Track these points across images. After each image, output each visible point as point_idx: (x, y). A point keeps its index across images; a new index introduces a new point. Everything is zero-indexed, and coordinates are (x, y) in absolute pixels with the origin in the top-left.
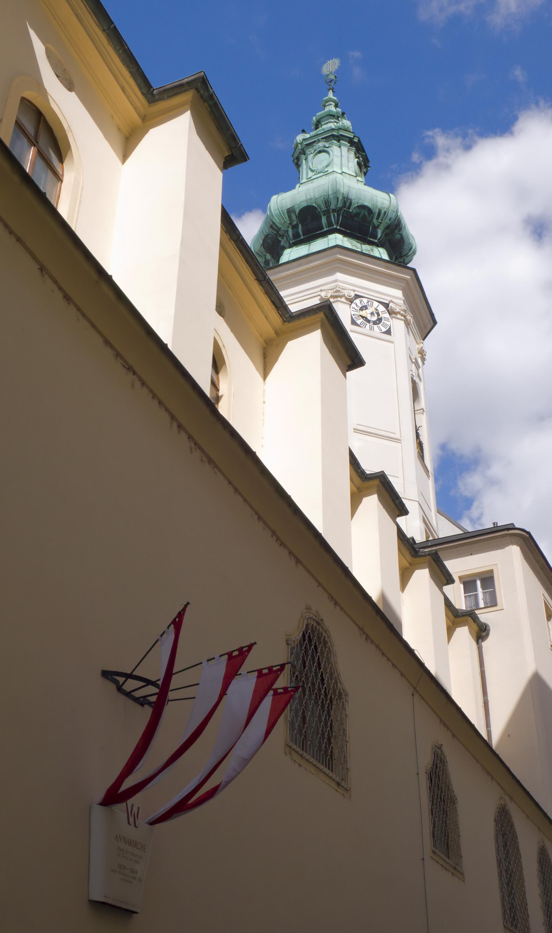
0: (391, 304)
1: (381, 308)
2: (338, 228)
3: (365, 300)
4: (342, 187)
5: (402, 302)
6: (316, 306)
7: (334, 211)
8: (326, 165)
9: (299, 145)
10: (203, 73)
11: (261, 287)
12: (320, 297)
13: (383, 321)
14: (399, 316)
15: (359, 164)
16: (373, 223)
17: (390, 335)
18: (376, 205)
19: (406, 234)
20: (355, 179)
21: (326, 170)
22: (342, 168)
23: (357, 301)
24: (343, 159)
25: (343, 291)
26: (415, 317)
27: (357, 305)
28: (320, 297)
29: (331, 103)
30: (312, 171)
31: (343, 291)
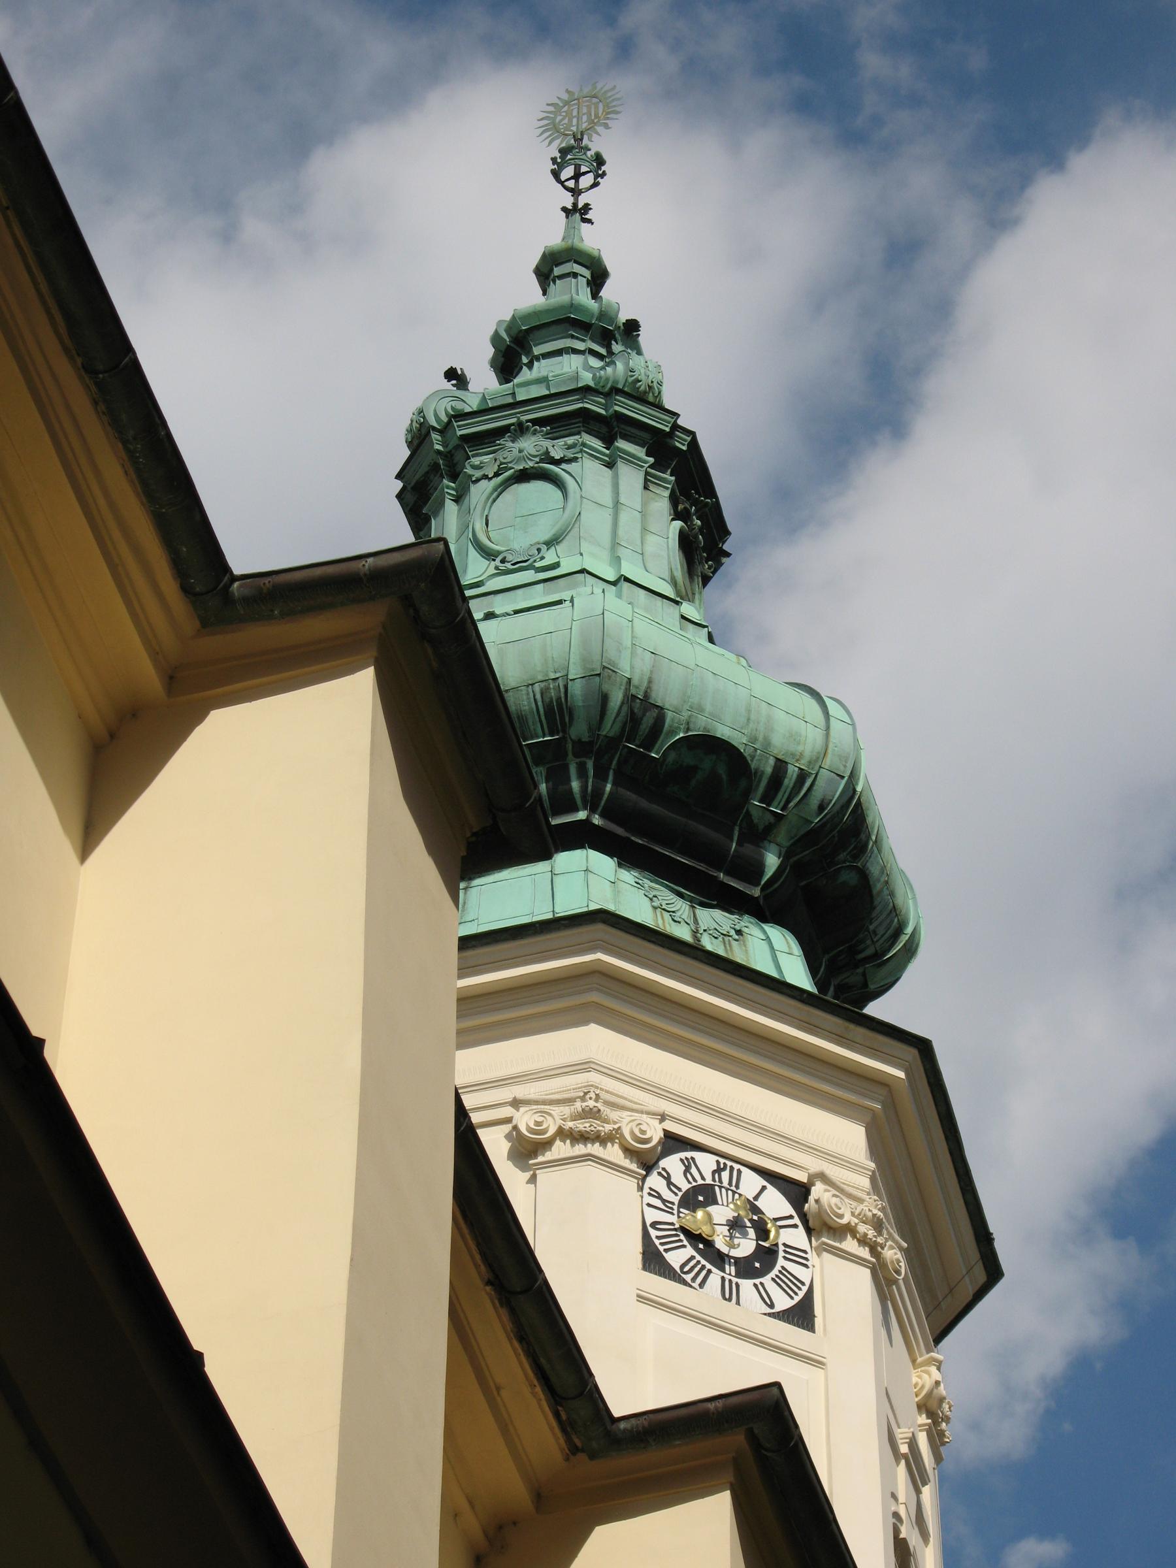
0: (818, 1191)
1: (775, 1204)
2: (597, 820)
3: (706, 1163)
4: (626, 654)
5: (865, 1183)
6: (719, 1404)
7: (583, 749)
8: (547, 536)
9: (435, 436)
10: (441, 546)
11: (504, 1312)
12: (507, 1128)
13: (781, 1262)
14: (850, 1245)
15: (686, 542)
16: (748, 814)
17: (814, 1332)
18: (767, 743)
19: (883, 868)
20: (671, 614)
21: (550, 558)
22: (616, 561)
23: (673, 1163)
24: (624, 517)
25: (614, 1115)
26: (913, 1254)
27: (670, 1183)
28: (507, 1128)
29: (577, 268)
30: (489, 554)
31: (614, 1115)
